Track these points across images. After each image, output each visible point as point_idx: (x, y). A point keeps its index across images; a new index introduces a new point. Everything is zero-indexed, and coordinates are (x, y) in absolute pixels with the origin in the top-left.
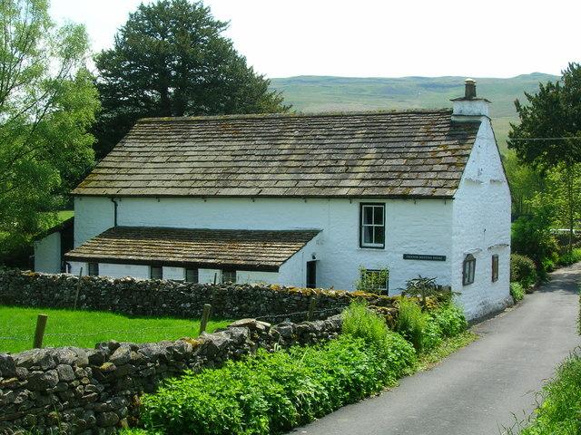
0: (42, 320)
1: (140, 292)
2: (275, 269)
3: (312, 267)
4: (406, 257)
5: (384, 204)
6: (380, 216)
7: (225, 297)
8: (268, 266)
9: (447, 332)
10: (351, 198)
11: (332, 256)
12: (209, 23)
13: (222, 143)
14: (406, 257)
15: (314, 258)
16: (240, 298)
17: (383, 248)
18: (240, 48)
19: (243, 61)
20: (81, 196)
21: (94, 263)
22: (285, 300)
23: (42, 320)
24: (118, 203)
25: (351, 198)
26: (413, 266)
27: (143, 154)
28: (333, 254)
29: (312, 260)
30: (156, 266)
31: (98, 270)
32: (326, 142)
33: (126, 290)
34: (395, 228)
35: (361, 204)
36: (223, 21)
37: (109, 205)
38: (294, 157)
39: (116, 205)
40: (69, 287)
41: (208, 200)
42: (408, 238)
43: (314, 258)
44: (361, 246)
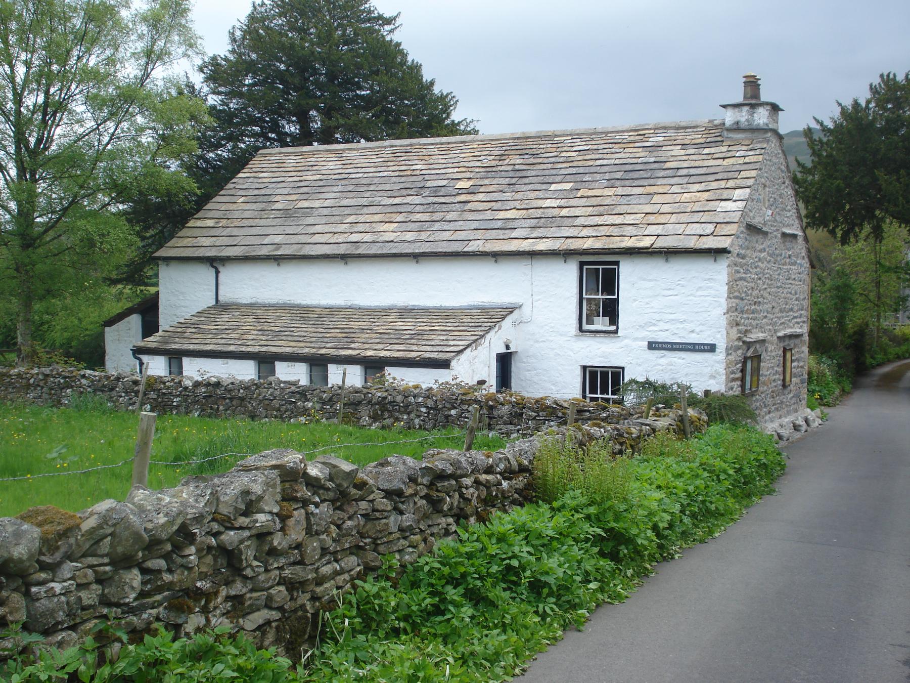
0: (712, 348)
1: (231, 399)
2: (445, 364)
3: (505, 361)
4: (652, 346)
5: (617, 263)
6: (610, 282)
7: (361, 408)
8: (408, 359)
9: (390, 553)
10: (566, 255)
11: (537, 345)
12: (369, 20)
13: (714, 185)
14: (652, 346)
15: (508, 347)
16: (384, 409)
17: (616, 332)
18: (761, 91)
19: (416, 69)
20: (168, 260)
21: (175, 357)
22: (453, 412)
23: (712, 348)
24: (221, 269)
25: (566, 255)
26: (663, 361)
27: (261, 199)
28: (537, 342)
29: (503, 350)
30: (266, 361)
31: (182, 368)
32: (529, 173)
33: (210, 396)
34: (635, 300)
35: (582, 264)
36: (387, 15)
37: (208, 274)
38: (481, 197)
39: (217, 272)
40: (126, 392)
41: (499, 258)
42: (657, 317)
43: (508, 347)
44: (581, 329)
